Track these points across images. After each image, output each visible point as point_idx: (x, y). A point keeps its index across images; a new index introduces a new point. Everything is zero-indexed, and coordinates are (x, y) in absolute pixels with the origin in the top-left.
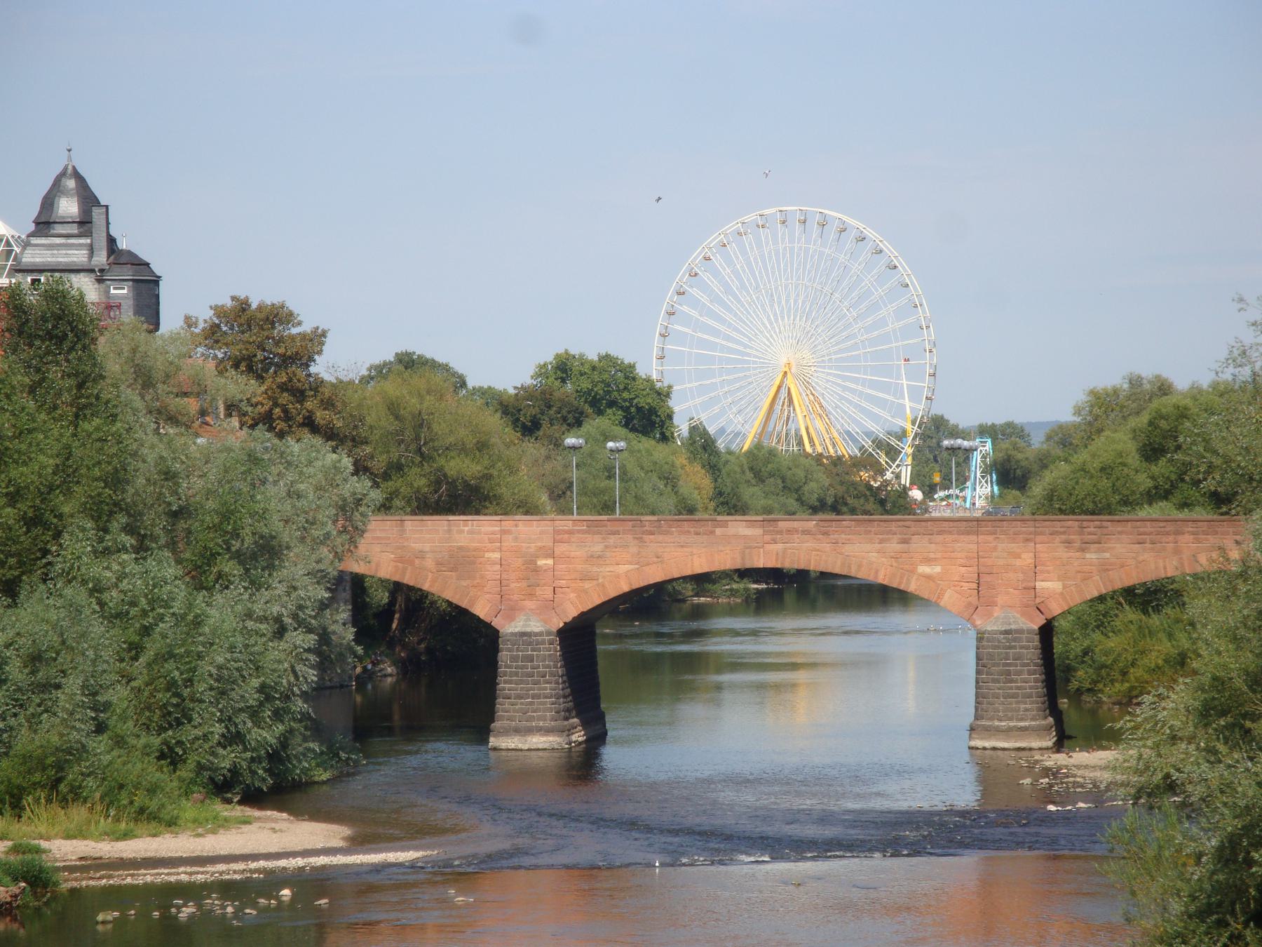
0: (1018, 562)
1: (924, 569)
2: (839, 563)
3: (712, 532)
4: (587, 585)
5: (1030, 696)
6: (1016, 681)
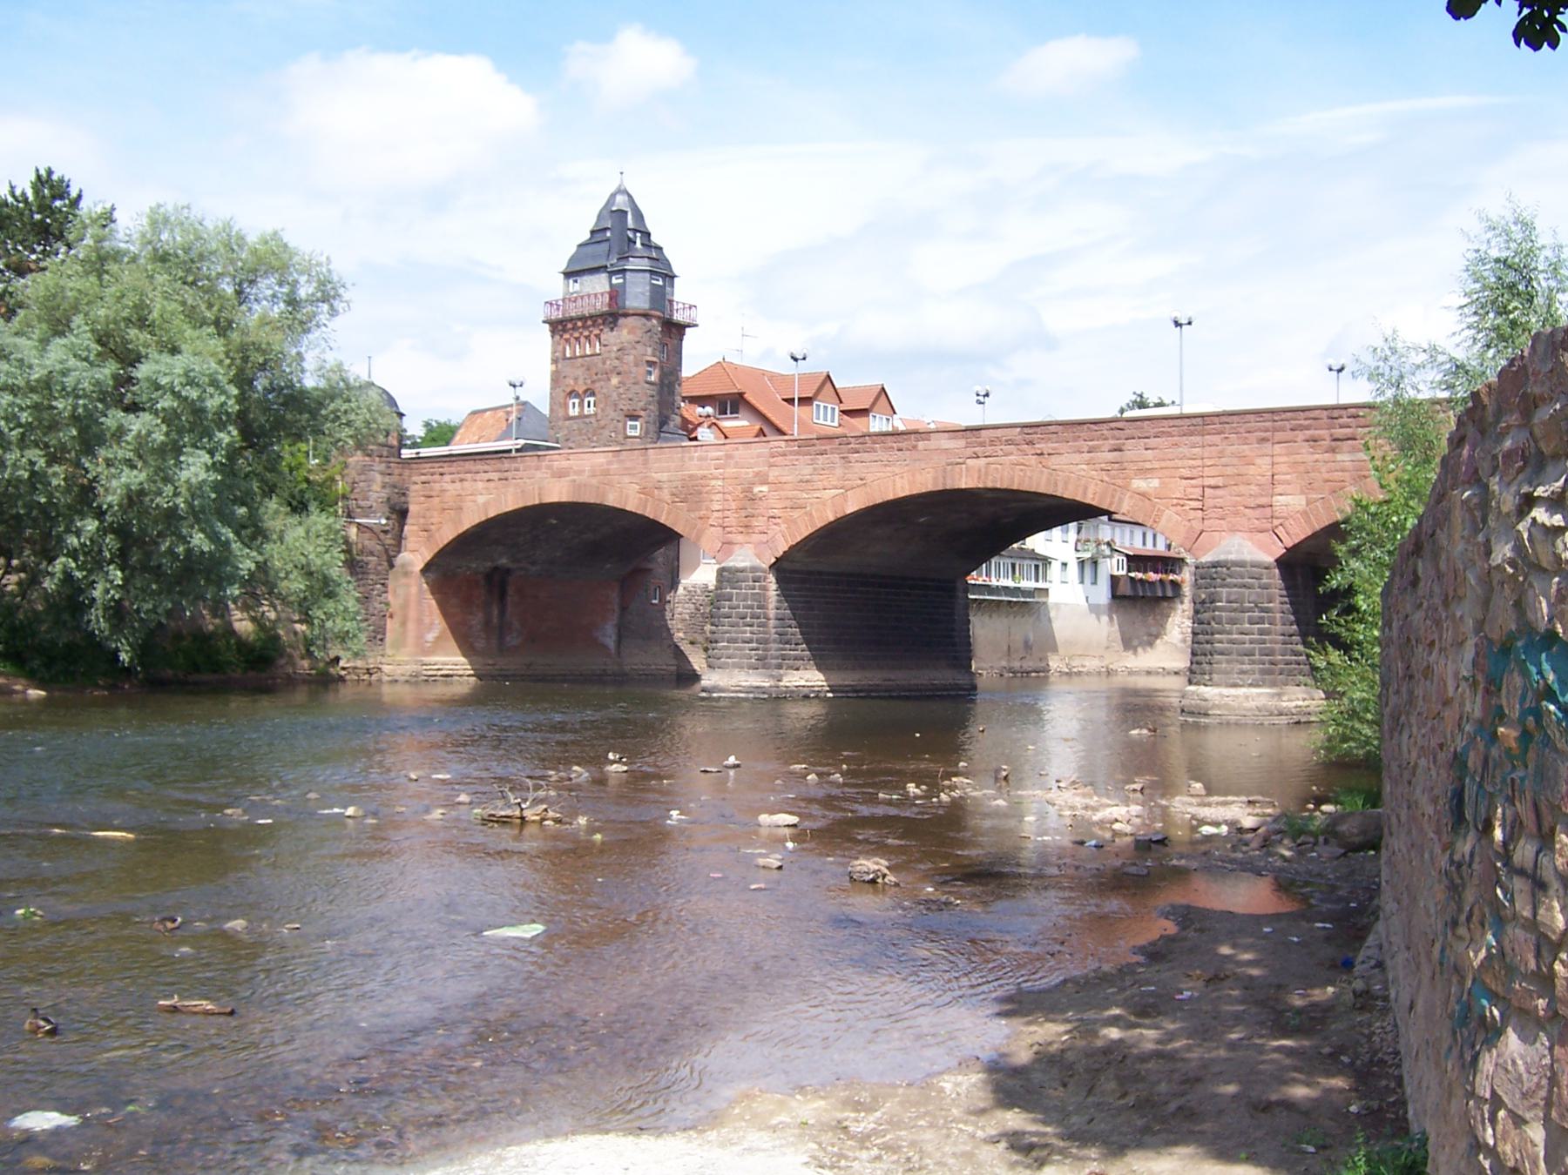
0: (1252, 470)
1: (1139, 484)
2: (1044, 478)
3: (915, 447)
4: (796, 514)
5: (1250, 654)
6: (1229, 633)
